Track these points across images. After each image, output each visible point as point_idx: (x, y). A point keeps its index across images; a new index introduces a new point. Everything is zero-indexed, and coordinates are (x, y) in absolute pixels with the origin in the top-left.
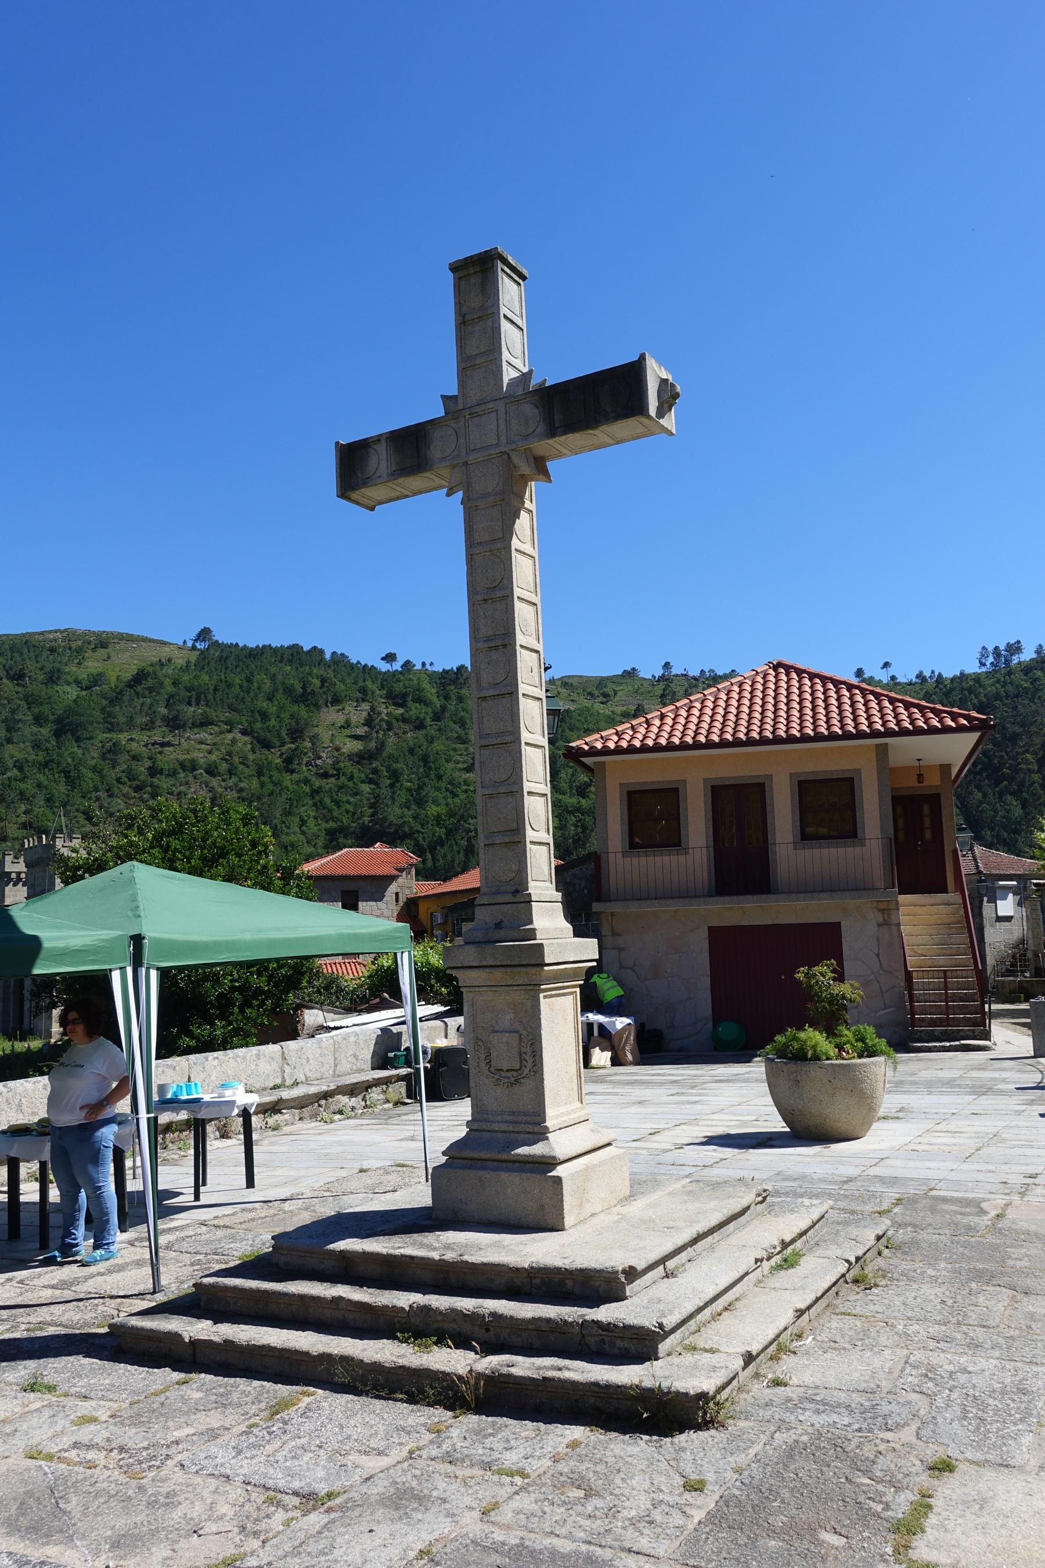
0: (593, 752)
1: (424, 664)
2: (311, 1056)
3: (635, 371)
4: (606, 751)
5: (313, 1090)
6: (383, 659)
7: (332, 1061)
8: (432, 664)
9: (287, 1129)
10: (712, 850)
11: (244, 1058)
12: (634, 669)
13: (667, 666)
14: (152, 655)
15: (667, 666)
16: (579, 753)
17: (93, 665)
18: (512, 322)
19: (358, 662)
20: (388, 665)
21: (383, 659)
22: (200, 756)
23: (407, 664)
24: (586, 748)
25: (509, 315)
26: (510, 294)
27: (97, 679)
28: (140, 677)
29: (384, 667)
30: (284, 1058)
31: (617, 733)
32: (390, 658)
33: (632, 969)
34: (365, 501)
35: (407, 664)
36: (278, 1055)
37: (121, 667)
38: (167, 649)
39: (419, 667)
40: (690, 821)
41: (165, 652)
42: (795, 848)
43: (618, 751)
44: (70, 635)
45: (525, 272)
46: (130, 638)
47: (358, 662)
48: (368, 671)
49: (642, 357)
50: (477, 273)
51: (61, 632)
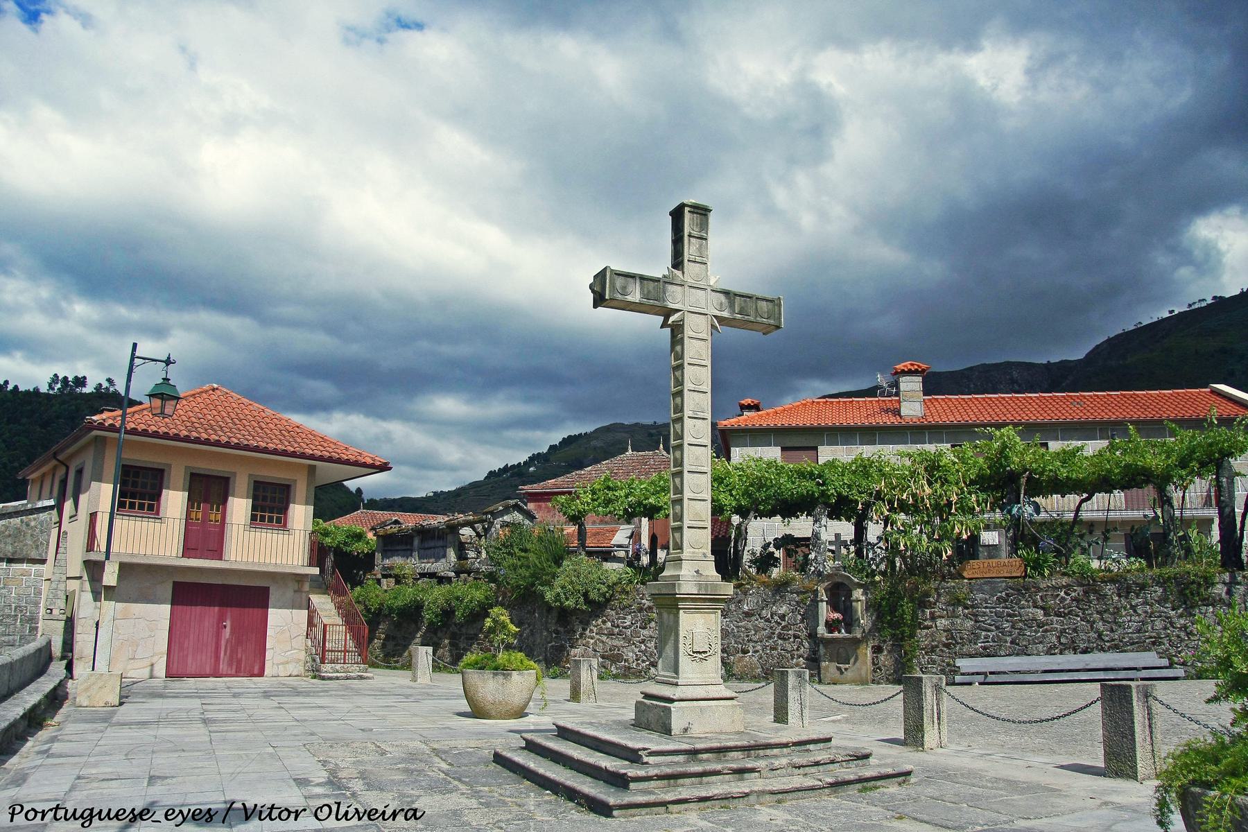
25: (694, 335)
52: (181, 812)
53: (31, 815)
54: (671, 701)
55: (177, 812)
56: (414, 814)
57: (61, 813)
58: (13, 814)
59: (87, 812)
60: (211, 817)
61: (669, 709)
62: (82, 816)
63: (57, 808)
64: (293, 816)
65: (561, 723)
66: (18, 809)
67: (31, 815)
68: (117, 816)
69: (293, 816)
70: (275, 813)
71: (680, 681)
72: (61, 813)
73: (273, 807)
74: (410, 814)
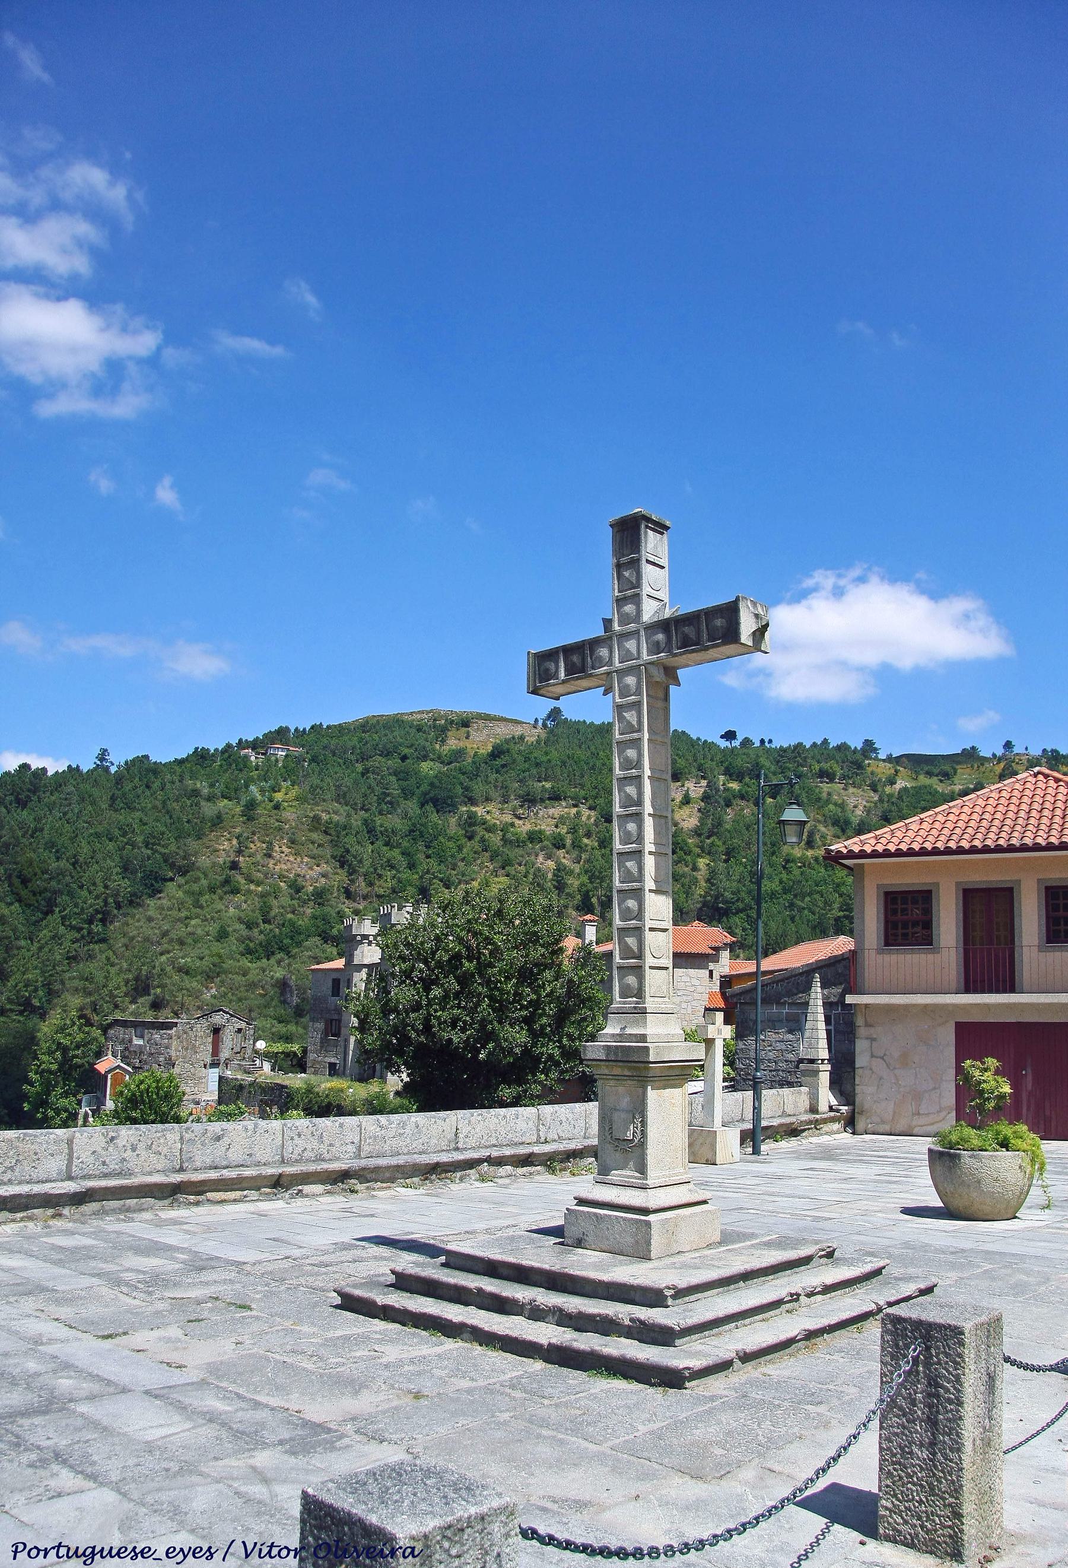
0: (851, 855)
1: (762, 741)
2: (564, 1119)
3: (731, 611)
4: (862, 854)
5: (561, 1147)
6: (722, 737)
7: (583, 1125)
8: (770, 741)
9: (537, 1178)
10: (1017, 943)
11: (505, 1117)
12: (973, 748)
13: (1008, 745)
14: (503, 731)
15: (1008, 745)
16: (839, 855)
17: (453, 743)
18: (654, 564)
19: (699, 739)
20: (728, 744)
21: (722, 737)
22: (547, 827)
23: (746, 742)
24: (845, 851)
25: (652, 558)
26: (653, 544)
27: (459, 754)
28: (497, 753)
29: (723, 744)
30: (539, 1119)
31: (876, 837)
32: (730, 735)
33: (882, 1058)
34: (550, 695)
35: (746, 742)
36: (534, 1118)
37: (480, 742)
38: (520, 728)
39: (757, 744)
40: (942, 921)
41: (518, 731)
42: (1039, 951)
43: (875, 854)
44: (435, 716)
45: (668, 523)
46: (487, 718)
47: (699, 739)
48: (708, 746)
49: (736, 602)
50: (628, 532)
51: (428, 712)
52: (182, 1550)
53: (34, 1553)
54: (645, 1211)
55: (178, 1550)
56: (412, 1553)
57: (63, 1551)
58: (16, 1552)
59: (90, 1550)
60: (212, 1555)
61: (648, 1224)
62: (84, 1554)
63: (60, 1545)
64: (42, 1553)
65: (399, 1269)
66: (21, 1547)
67: (34, 1553)
68: (118, 1554)
69: (42, 1553)
70: (275, 1551)
71: (650, 1182)
72: (63, 1551)
73: (272, 1546)
74: (265, 1551)
